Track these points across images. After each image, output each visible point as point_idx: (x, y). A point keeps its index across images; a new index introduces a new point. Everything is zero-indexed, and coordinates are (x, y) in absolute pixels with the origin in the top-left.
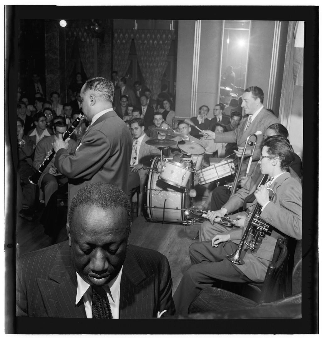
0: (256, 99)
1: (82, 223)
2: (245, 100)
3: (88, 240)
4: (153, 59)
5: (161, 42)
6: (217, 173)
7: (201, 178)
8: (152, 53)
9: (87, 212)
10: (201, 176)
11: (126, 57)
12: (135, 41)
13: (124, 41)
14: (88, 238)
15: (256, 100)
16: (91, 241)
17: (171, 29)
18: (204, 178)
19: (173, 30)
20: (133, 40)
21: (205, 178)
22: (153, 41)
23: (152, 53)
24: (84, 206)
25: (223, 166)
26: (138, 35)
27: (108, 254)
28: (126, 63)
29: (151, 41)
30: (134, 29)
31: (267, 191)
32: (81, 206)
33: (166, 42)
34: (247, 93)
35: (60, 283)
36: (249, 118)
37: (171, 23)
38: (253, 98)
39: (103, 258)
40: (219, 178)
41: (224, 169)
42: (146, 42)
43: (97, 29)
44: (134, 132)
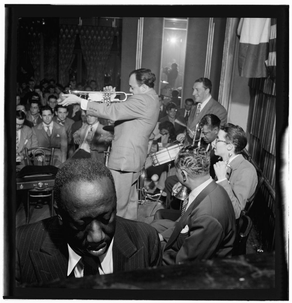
0: (206, 89)
1: (73, 201)
2: (196, 89)
3: (83, 215)
4: (97, 53)
5: (104, 38)
6: (169, 155)
7: (154, 160)
8: (96, 48)
9: (75, 189)
10: (155, 158)
11: (71, 51)
12: (80, 36)
13: (69, 36)
14: (83, 213)
15: (206, 90)
16: (85, 215)
17: (113, 26)
18: (157, 161)
19: (115, 27)
20: (78, 35)
21: (158, 160)
22: (97, 37)
23: (96, 48)
24: (69, 185)
25: (175, 149)
26: (82, 31)
27: (103, 225)
28: (71, 56)
29: (95, 37)
30: (78, 25)
31: (226, 167)
32: (67, 185)
33: (109, 37)
34: (199, 83)
35: (51, 254)
36: (198, 106)
37: (114, 21)
38: (204, 88)
39: (99, 229)
40: (171, 160)
41: (175, 151)
42: (90, 37)
43: (44, 23)
44: (89, 119)
